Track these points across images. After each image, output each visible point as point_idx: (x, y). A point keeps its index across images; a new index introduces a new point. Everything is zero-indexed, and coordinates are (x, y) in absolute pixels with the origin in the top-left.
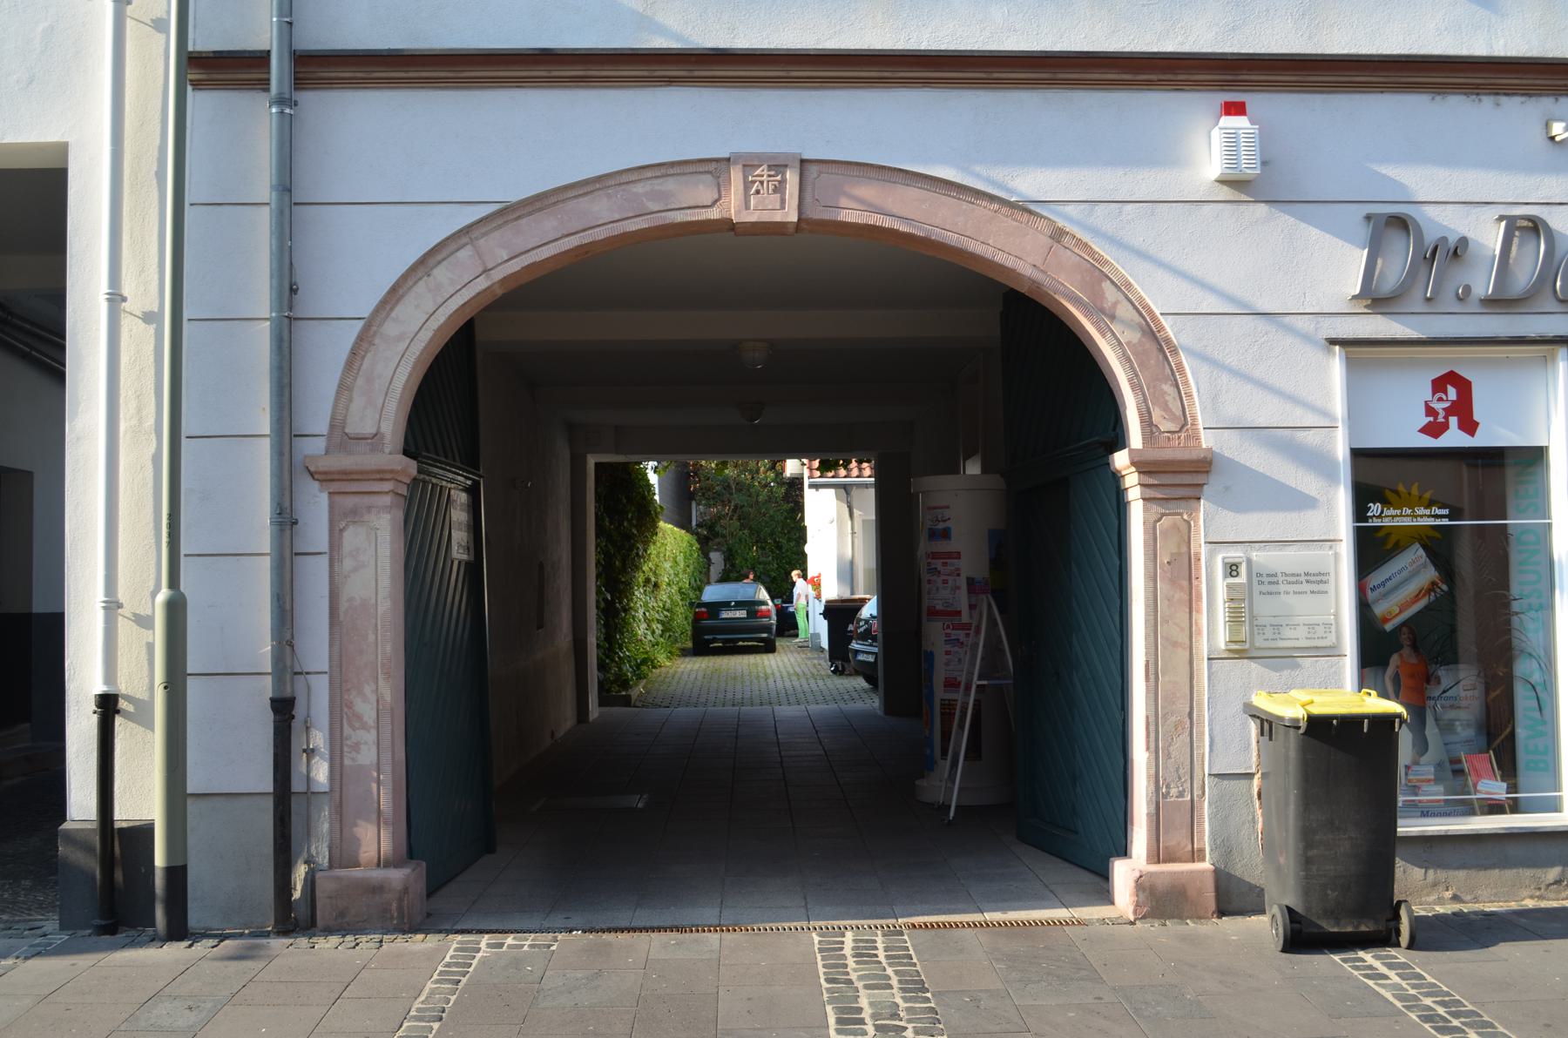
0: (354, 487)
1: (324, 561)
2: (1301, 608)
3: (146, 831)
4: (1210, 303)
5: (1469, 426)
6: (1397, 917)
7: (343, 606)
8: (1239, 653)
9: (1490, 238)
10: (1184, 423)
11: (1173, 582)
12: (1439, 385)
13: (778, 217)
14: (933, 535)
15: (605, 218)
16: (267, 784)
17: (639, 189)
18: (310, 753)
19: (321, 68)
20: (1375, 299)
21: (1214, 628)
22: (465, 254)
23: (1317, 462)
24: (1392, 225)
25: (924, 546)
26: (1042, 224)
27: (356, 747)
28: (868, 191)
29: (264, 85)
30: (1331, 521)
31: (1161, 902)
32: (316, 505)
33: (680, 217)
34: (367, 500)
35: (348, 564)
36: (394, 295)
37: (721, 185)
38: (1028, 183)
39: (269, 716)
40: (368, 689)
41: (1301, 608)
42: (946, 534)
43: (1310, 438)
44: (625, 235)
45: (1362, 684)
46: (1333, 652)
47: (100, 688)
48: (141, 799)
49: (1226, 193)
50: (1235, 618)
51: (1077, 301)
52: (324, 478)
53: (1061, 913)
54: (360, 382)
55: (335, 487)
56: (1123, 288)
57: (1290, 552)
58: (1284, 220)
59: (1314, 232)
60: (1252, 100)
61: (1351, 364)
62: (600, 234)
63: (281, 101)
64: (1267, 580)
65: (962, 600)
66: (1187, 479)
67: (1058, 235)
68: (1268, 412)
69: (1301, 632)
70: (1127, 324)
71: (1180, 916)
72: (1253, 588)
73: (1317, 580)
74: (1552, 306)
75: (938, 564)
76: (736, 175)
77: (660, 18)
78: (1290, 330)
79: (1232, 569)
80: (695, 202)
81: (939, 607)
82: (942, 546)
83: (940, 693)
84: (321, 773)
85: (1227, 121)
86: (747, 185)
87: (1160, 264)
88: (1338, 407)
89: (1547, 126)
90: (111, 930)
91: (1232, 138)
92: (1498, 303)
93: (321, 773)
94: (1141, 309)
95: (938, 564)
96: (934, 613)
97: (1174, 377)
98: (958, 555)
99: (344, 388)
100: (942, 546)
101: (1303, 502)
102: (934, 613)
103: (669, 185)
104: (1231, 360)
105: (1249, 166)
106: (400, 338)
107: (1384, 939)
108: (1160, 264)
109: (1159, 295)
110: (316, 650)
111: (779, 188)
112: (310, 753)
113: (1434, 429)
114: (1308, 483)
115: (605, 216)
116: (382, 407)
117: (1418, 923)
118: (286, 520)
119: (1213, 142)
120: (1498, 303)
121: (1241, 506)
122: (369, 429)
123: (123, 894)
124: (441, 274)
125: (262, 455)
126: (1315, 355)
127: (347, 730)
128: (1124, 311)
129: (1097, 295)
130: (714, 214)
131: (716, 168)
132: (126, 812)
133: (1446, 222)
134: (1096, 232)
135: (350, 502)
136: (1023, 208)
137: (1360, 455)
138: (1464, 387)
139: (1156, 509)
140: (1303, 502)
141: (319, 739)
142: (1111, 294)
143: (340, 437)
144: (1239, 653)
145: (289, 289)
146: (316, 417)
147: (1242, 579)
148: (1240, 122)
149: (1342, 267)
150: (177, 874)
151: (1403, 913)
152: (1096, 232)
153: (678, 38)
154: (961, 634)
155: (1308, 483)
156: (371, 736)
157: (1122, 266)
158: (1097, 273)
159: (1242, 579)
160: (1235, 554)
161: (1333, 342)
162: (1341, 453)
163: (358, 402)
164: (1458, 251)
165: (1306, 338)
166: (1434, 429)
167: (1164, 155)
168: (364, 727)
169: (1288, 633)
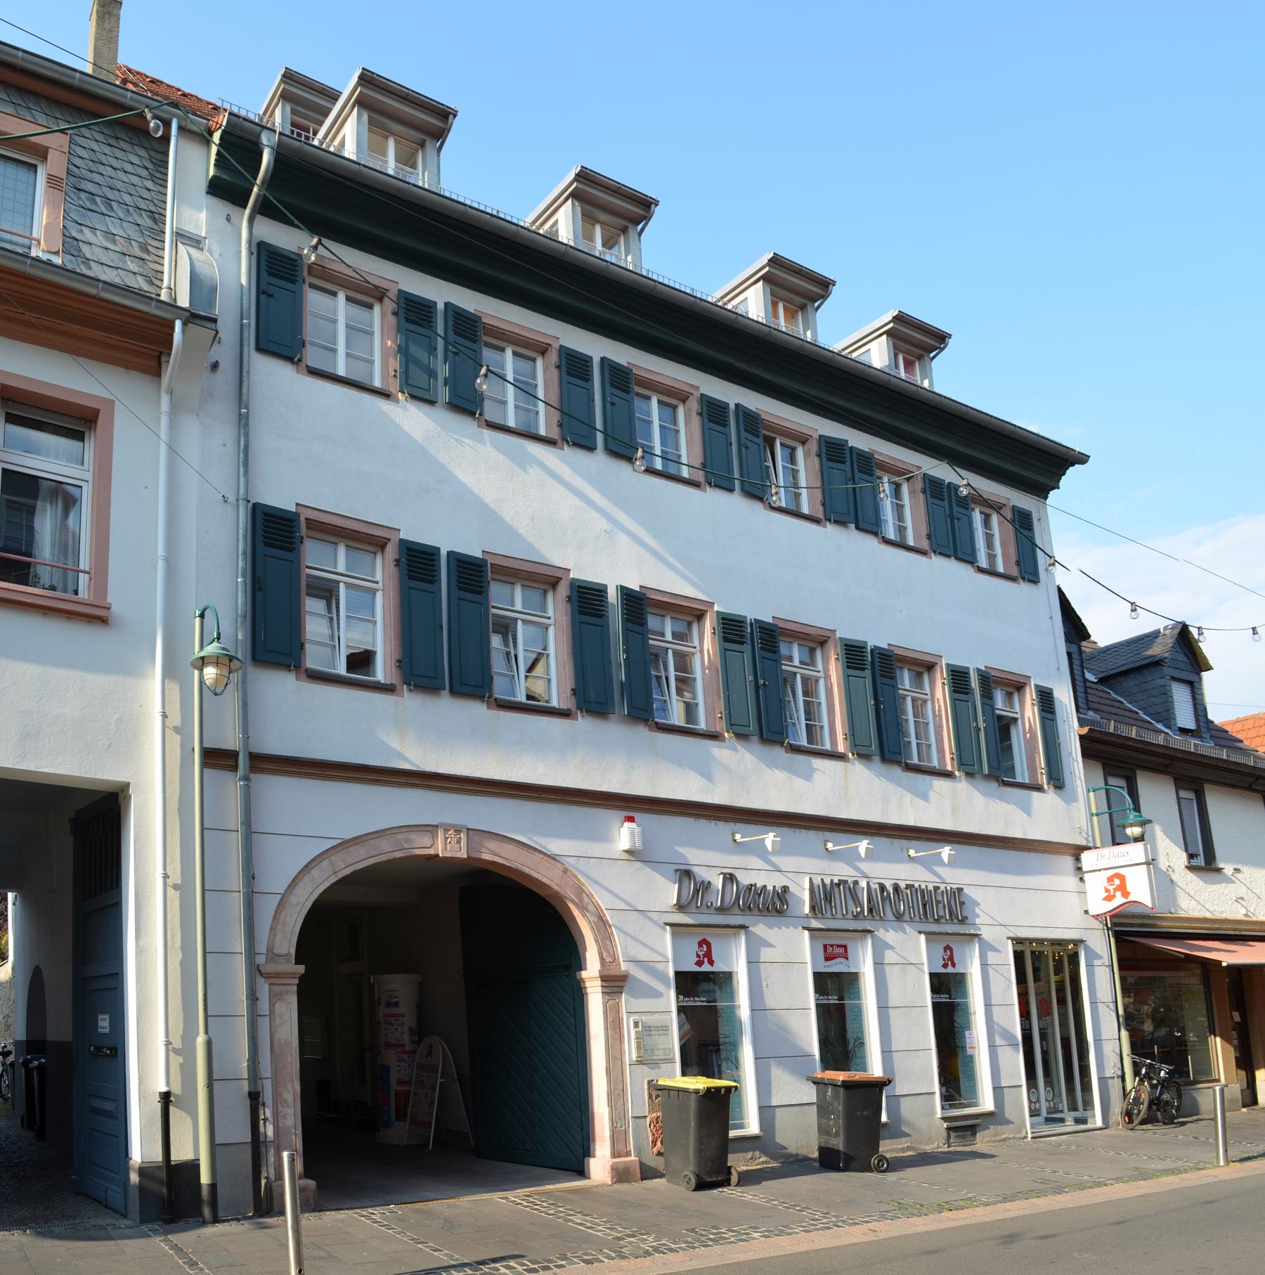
0: (281, 981)
1: (267, 1019)
2: (660, 1040)
3: (194, 1166)
4: (622, 906)
5: (711, 963)
6: (729, 1173)
7: (276, 1043)
8: (640, 1062)
9: (718, 883)
10: (615, 959)
11: (614, 1030)
12: (700, 944)
13: (458, 855)
14: (389, 1005)
15: (386, 851)
16: (248, 1138)
17: (400, 837)
18: (265, 1120)
19: (265, 763)
20: (681, 907)
21: (630, 1052)
22: (325, 863)
23: (662, 977)
24: (685, 874)
25: (382, 1011)
26: (559, 865)
27: (284, 1117)
28: (492, 844)
29: (235, 768)
30: (669, 1004)
31: (621, 1175)
32: (264, 988)
33: (418, 852)
34: (286, 988)
35: (278, 1021)
36: (294, 883)
37: (434, 837)
38: (555, 846)
39: (248, 1102)
40: (289, 1086)
41: (660, 1040)
42: (396, 1005)
43: (659, 966)
44: (395, 859)
45: (684, 1074)
46: (672, 1061)
47: (164, 1089)
48: (191, 1144)
49: (626, 856)
50: (639, 1047)
51: (574, 903)
52: (267, 976)
53: (551, 1187)
54: (280, 926)
55: (272, 981)
56: (590, 896)
57: (656, 1016)
58: (647, 870)
59: (657, 875)
60: (637, 815)
61: (674, 934)
62: (384, 858)
63: (246, 778)
64: (648, 1028)
65: (406, 1039)
66: (618, 984)
67: (565, 871)
68: (644, 955)
69: (661, 1052)
70: (592, 914)
71: (627, 1181)
72: (646, 1032)
73: (665, 1029)
74: (738, 912)
75: (392, 1020)
76: (440, 833)
77: (407, 754)
78: (650, 919)
79: (636, 1024)
80: (423, 846)
81: (393, 1042)
82: (396, 1011)
83: (394, 1086)
84: (270, 1131)
85: (627, 824)
86: (446, 839)
87: (602, 887)
88: (670, 955)
89: (733, 835)
90: (171, 1221)
91: (632, 833)
92: (722, 910)
93: (270, 1131)
94: (597, 907)
95: (392, 1020)
96: (388, 1045)
97: (609, 937)
98: (403, 1016)
99: (273, 929)
100: (396, 1011)
101: (658, 995)
102: (388, 1045)
103: (413, 836)
104: (631, 932)
105: (639, 845)
106: (297, 905)
107: (726, 1182)
108: (602, 887)
109: (603, 901)
110: (266, 1069)
111: (459, 842)
112: (265, 1120)
113: (699, 963)
114: (659, 987)
115: (386, 849)
116: (287, 943)
117: (740, 1174)
118: (253, 998)
119: (625, 835)
120: (722, 910)
121: (636, 996)
122: (285, 951)
123: (175, 1198)
124: (315, 873)
125: (240, 964)
126: (658, 930)
127: (280, 1108)
128: (591, 907)
129: (581, 899)
130: (432, 852)
131: (431, 829)
132: (181, 1153)
133: (702, 873)
134: (581, 872)
135: (278, 989)
136: (553, 858)
137: (678, 974)
138: (709, 945)
139: (607, 997)
140: (658, 995)
141: (268, 1113)
142: (586, 899)
143: (273, 956)
144: (640, 1062)
145: (250, 876)
146: (262, 947)
147: (640, 1029)
148: (633, 825)
149: (670, 893)
150: (213, 1187)
151: (733, 1171)
152: (581, 872)
153: (413, 764)
154: (405, 1056)
155: (659, 987)
156: (291, 1111)
157: (590, 888)
158: (580, 890)
159: (640, 1029)
160: (637, 1017)
161: (667, 924)
162: (671, 974)
163: (279, 937)
164: (707, 886)
165: (656, 923)
166: (699, 963)
167: (603, 837)
168: (288, 1106)
169: (656, 1053)
